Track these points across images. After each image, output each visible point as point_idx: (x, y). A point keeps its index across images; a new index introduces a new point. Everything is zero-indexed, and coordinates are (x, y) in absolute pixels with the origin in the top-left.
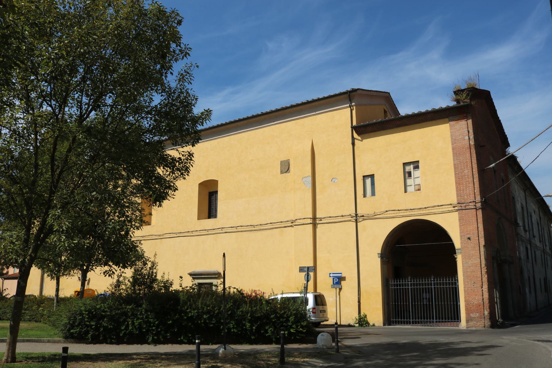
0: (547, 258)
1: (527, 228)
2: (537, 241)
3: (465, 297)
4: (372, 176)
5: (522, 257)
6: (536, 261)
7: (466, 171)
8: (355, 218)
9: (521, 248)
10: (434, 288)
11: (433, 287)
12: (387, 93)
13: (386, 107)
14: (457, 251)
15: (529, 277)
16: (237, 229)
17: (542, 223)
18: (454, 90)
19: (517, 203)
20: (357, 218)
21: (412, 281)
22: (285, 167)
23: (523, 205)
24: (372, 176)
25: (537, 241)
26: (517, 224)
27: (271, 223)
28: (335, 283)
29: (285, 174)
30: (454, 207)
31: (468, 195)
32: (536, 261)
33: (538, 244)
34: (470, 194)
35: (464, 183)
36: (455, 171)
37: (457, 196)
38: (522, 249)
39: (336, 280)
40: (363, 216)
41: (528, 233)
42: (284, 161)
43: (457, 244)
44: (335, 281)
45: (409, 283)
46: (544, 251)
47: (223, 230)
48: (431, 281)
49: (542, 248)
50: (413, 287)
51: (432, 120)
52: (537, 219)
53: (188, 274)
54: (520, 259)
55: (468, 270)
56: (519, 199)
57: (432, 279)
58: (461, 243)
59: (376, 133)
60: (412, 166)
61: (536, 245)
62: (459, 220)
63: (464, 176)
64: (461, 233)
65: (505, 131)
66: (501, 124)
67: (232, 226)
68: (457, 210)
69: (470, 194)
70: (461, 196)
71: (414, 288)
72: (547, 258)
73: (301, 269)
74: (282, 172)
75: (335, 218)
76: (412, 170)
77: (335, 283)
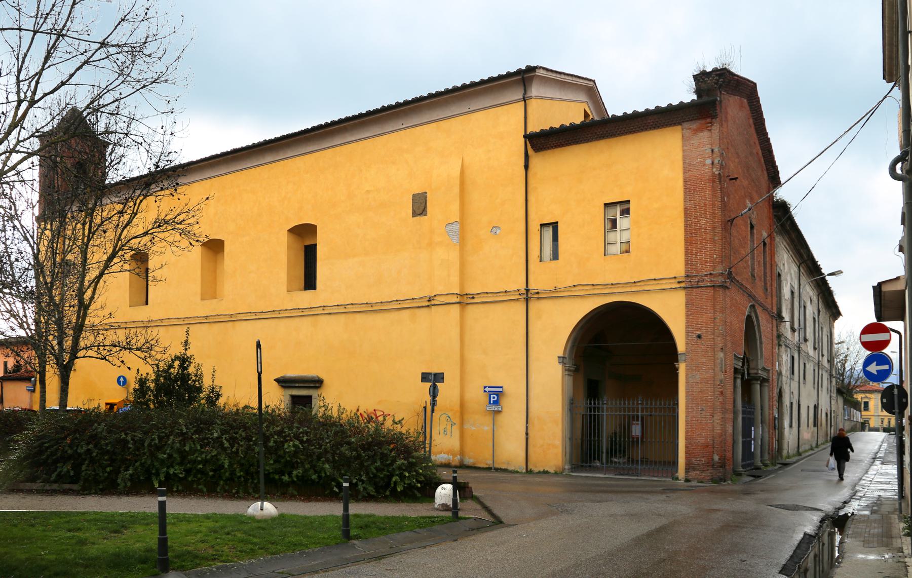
0: (822, 375)
1: (796, 326)
2: (809, 348)
3: (687, 432)
4: (555, 226)
5: (784, 372)
6: (804, 378)
7: (703, 222)
8: (525, 296)
11: (640, 414)
12: (591, 80)
13: (589, 106)
15: (792, 403)
16: (347, 310)
18: (695, 73)
19: (784, 283)
20: (528, 296)
21: (645, 403)
22: (420, 206)
23: (794, 288)
24: (555, 226)
25: (809, 348)
26: (780, 318)
27: (397, 301)
29: (418, 218)
30: (679, 282)
31: (704, 263)
32: (804, 378)
33: (811, 352)
34: (706, 262)
35: (699, 242)
36: (686, 221)
37: (687, 264)
38: (785, 358)
39: (494, 398)
40: (538, 293)
42: (419, 194)
43: (681, 346)
44: (492, 400)
45: (640, 406)
46: (819, 364)
47: (325, 311)
48: (638, 404)
52: (814, 313)
53: (275, 380)
54: (780, 374)
55: (695, 389)
56: (789, 278)
58: (687, 344)
60: (618, 209)
61: (808, 354)
62: (687, 304)
64: (687, 327)
65: (776, 159)
66: (770, 145)
67: (339, 304)
68: (684, 288)
69: (706, 262)
70: (692, 265)
72: (822, 375)
73: (425, 377)
74: (415, 214)
75: (495, 295)
76: (618, 217)
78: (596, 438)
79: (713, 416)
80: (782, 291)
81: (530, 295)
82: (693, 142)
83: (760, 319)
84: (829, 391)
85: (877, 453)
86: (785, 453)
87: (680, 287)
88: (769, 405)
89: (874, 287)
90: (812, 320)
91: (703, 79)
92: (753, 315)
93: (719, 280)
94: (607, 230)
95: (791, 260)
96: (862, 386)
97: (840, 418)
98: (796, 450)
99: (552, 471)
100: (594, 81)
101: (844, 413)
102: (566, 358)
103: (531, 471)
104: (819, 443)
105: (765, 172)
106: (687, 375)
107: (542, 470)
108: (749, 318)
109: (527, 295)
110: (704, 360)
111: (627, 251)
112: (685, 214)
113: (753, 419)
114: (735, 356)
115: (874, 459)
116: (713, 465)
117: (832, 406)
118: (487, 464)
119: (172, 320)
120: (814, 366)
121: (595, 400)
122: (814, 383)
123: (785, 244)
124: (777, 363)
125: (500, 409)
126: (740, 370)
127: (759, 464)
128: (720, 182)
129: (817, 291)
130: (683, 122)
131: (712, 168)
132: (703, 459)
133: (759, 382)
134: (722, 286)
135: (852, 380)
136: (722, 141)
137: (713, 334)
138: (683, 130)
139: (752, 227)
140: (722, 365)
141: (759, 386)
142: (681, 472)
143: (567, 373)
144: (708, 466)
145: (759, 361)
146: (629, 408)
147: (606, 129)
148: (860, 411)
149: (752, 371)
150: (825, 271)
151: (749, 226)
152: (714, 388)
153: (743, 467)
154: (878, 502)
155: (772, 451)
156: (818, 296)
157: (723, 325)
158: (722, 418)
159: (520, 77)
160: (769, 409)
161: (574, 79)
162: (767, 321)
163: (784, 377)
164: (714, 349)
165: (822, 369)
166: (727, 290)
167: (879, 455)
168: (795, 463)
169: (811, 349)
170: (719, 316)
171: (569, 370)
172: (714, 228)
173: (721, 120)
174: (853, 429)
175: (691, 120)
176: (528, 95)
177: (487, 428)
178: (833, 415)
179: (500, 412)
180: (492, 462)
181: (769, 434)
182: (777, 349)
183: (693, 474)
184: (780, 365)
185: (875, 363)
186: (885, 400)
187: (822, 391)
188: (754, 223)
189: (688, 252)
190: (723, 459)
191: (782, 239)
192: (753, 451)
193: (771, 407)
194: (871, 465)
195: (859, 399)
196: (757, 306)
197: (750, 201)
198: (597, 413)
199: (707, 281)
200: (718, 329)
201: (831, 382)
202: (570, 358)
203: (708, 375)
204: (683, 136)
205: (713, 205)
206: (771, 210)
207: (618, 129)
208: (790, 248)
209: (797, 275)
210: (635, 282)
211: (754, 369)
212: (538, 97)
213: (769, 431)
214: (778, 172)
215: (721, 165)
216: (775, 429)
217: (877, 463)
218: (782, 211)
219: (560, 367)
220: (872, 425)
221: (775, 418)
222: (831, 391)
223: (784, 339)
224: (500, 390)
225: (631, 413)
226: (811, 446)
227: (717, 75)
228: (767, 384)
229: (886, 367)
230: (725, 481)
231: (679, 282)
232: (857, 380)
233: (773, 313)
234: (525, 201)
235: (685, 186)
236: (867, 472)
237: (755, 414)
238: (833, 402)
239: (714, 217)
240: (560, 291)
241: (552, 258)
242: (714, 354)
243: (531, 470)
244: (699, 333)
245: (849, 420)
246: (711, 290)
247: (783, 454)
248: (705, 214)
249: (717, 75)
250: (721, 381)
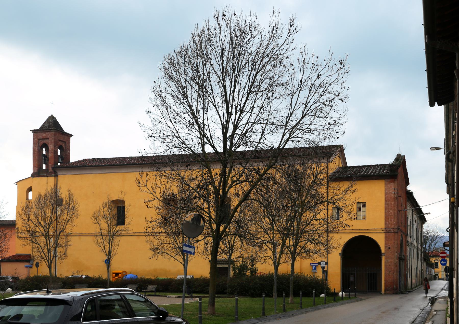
1: (411, 235)
3: (385, 279)
14: (382, 254)
15: (410, 267)
25: (415, 244)
30: (383, 230)
34: (392, 224)
36: (385, 211)
41: (411, 238)
43: (383, 250)
44: (314, 268)
46: (418, 248)
51: (375, 180)
58: (385, 250)
62: (385, 238)
63: (390, 214)
64: (385, 245)
68: (384, 232)
69: (392, 224)
70: (387, 225)
93: (396, 230)
97: (425, 272)
101: (427, 270)
110: (391, 255)
111: (365, 219)
119: (142, 233)
138: (385, 181)
148: (434, 269)
167: (444, 289)
172: (395, 214)
174: (431, 279)
179: (316, 272)
189: (386, 221)
190: (397, 287)
204: (385, 183)
215: (397, 194)
218: (410, 195)
219: (340, 257)
220: (440, 277)
229: (445, 262)
231: (383, 230)
248: (392, 209)
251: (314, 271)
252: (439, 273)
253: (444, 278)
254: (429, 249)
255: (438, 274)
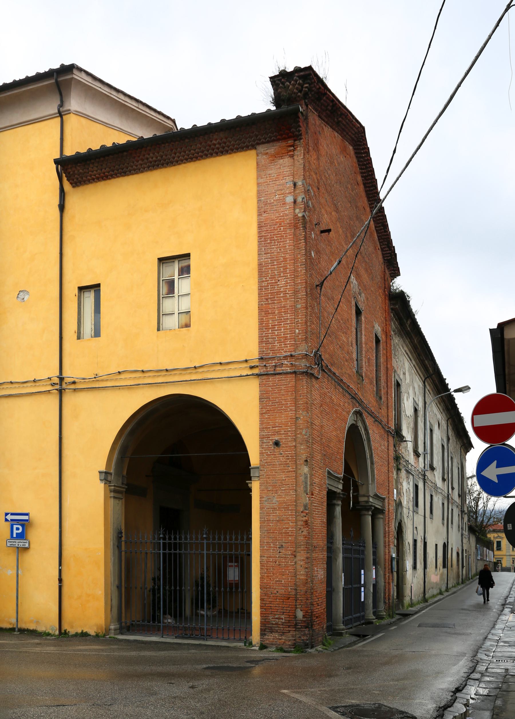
0: (452, 510)
1: (421, 450)
2: (437, 477)
3: (262, 578)
4: (96, 287)
5: (405, 503)
7: (282, 283)
9: (405, 484)
10: (163, 553)
15: (415, 541)
17: (451, 448)
19: (404, 396)
24: (96, 287)
28: (15, 536)
30: (252, 368)
33: (439, 483)
34: (286, 338)
36: (260, 282)
37: (261, 342)
38: (407, 486)
39: (18, 529)
40: (74, 383)
43: (254, 459)
44: (15, 532)
49: (446, 492)
50: (167, 551)
54: (399, 504)
55: (271, 518)
56: (411, 391)
57: (161, 536)
58: (261, 453)
59: (108, 182)
63: (278, 293)
64: (261, 430)
68: (258, 375)
69: (286, 338)
70: (267, 343)
71: (170, 554)
72: (452, 510)
75: (22, 385)
77: (15, 536)
78: (178, 588)
79: (295, 556)
80: (402, 405)
81: (64, 386)
82: (271, 172)
83: (370, 432)
84: (460, 528)
85: (507, 597)
86: (407, 600)
87: (253, 375)
88: (385, 542)
89: (491, 331)
90: (441, 447)
91: (283, 83)
92: (360, 424)
93: (303, 364)
94: (161, 296)
95: (414, 371)
96: (495, 524)
97: (472, 558)
98: (422, 595)
99: (92, 633)
100: (174, 121)
102: (111, 474)
103: (66, 633)
104: (450, 586)
105: (380, 252)
106: (261, 497)
107: (80, 631)
108: (353, 430)
109: (61, 385)
110: (283, 476)
111: (187, 326)
112: (259, 272)
113: (363, 559)
114: (329, 473)
115: (504, 605)
116: (296, 625)
117: (464, 545)
118: (10, 624)
120: (443, 500)
121: (175, 533)
122: (443, 519)
123: (406, 349)
124: (395, 490)
125: (27, 545)
126: (339, 493)
127: (371, 617)
128: (305, 227)
129: (446, 415)
130: (258, 144)
131: (294, 210)
132: (283, 617)
133: (370, 513)
134: (306, 373)
135: (485, 519)
136: (308, 174)
137: (295, 440)
138: (257, 155)
139: (358, 312)
140: (306, 483)
141: (370, 518)
142: (256, 637)
143: (112, 494)
144: (289, 627)
145: (370, 486)
146: (225, 545)
147: (161, 153)
148: (493, 551)
149: (361, 499)
150: (452, 386)
151: (354, 312)
152: (296, 516)
153: (345, 623)
154: (504, 687)
155: (389, 599)
156: (447, 421)
157: (308, 427)
158: (307, 558)
159: (53, 81)
160: (385, 547)
161: (141, 107)
162: (381, 436)
163: (404, 509)
164: (296, 461)
165: (452, 504)
166: (313, 380)
167: (509, 600)
168: (416, 613)
169: (439, 479)
170: (302, 414)
171: (115, 491)
172: (296, 292)
173: (307, 144)
175: (268, 142)
176: (66, 107)
177: (11, 572)
178: (465, 555)
180: (15, 620)
181: (385, 578)
182: (395, 473)
183: (270, 637)
184: (399, 493)
185: (495, 463)
186: (510, 527)
187: (452, 528)
188: (361, 306)
189: (263, 326)
191: (402, 342)
192: (362, 600)
193: (387, 545)
194: (500, 615)
195: (492, 539)
196: (365, 414)
197: (356, 278)
198: (178, 551)
199: (287, 366)
200: (301, 433)
201: (462, 518)
202: (115, 474)
203: (288, 498)
204: (258, 164)
205: (295, 260)
206: (387, 301)
207: (175, 154)
208: (413, 357)
209: (422, 391)
210: (195, 367)
211: (364, 496)
212: (78, 114)
213: (385, 575)
214: (395, 255)
216: (392, 572)
217: (507, 610)
219: (101, 487)
220: (504, 566)
221: (392, 559)
222: (462, 528)
223: (404, 463)
224: (26, 518)
225: (228, 552)
226: (440, 590)
227: (300, 77)
228: (381, 516)
230: (312, 647)
231: (252, 368)
232: (490, 518)
233: (389, 428)
234: (59, 255)
235: (259, 232)
236: (493, 627)
237: (366, 553)
238: (465, 541)
239: (296, 277)
240: (102, 380)
241: (93, 334)
242: (296, 467)
243: (65, 631)
244: (276, 438)
245: (481, 559)
246: (291, 378)
247: (405, 602)
248: (285, 272)
249: (300, 77)
250: (305, 506)
251: (20, 543)
252: (502, 558)
253: (511, 566)
254: (484, 511)
255: (500, 561)
